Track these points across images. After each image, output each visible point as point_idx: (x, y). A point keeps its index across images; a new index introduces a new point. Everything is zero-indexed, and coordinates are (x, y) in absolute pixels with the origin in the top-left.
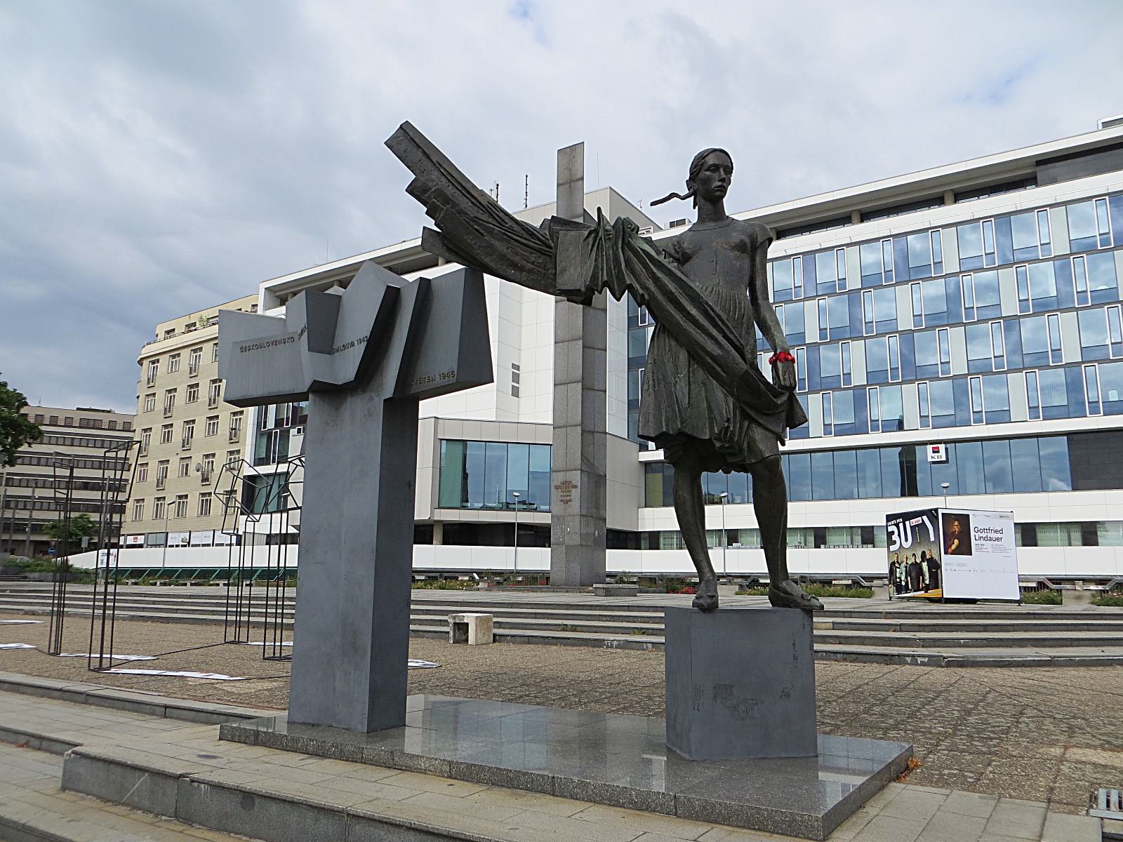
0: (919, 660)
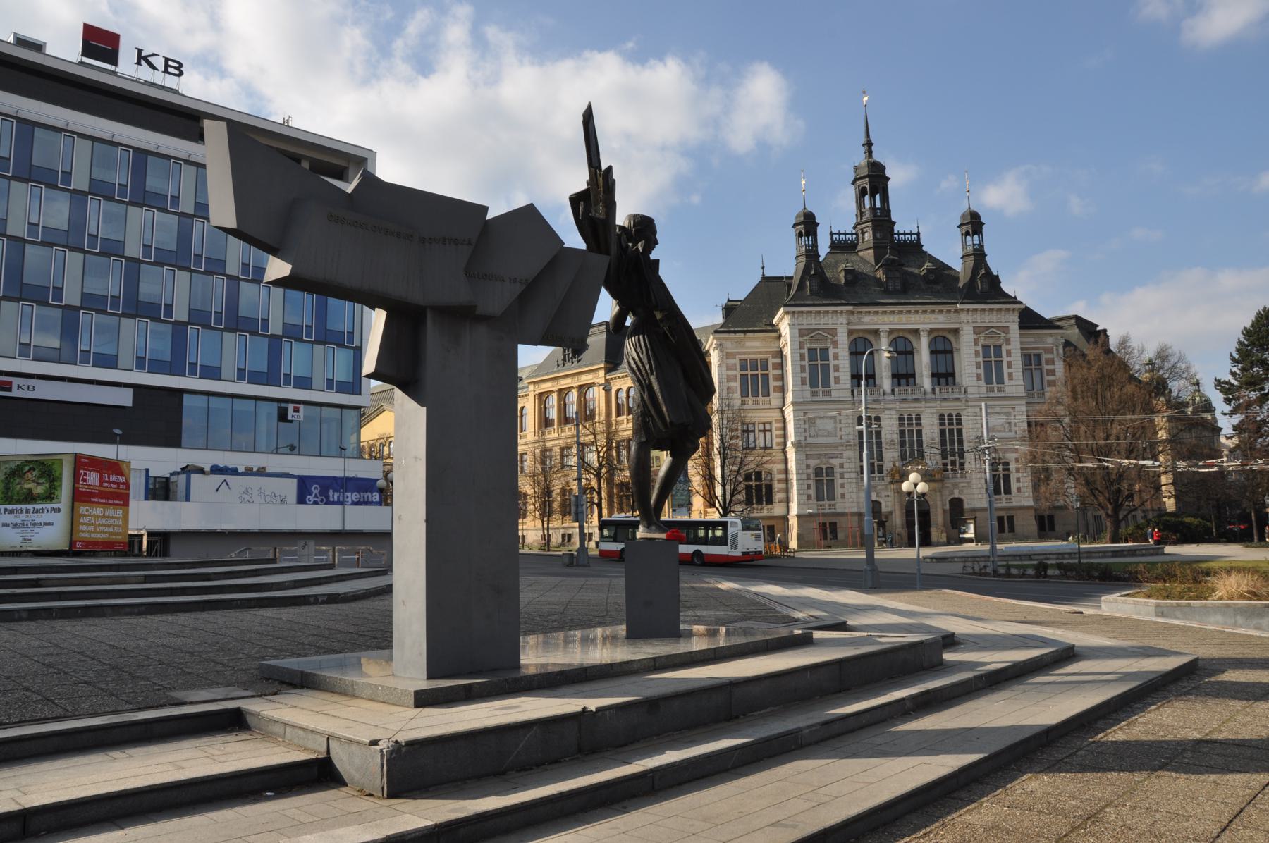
0: (320, 599)
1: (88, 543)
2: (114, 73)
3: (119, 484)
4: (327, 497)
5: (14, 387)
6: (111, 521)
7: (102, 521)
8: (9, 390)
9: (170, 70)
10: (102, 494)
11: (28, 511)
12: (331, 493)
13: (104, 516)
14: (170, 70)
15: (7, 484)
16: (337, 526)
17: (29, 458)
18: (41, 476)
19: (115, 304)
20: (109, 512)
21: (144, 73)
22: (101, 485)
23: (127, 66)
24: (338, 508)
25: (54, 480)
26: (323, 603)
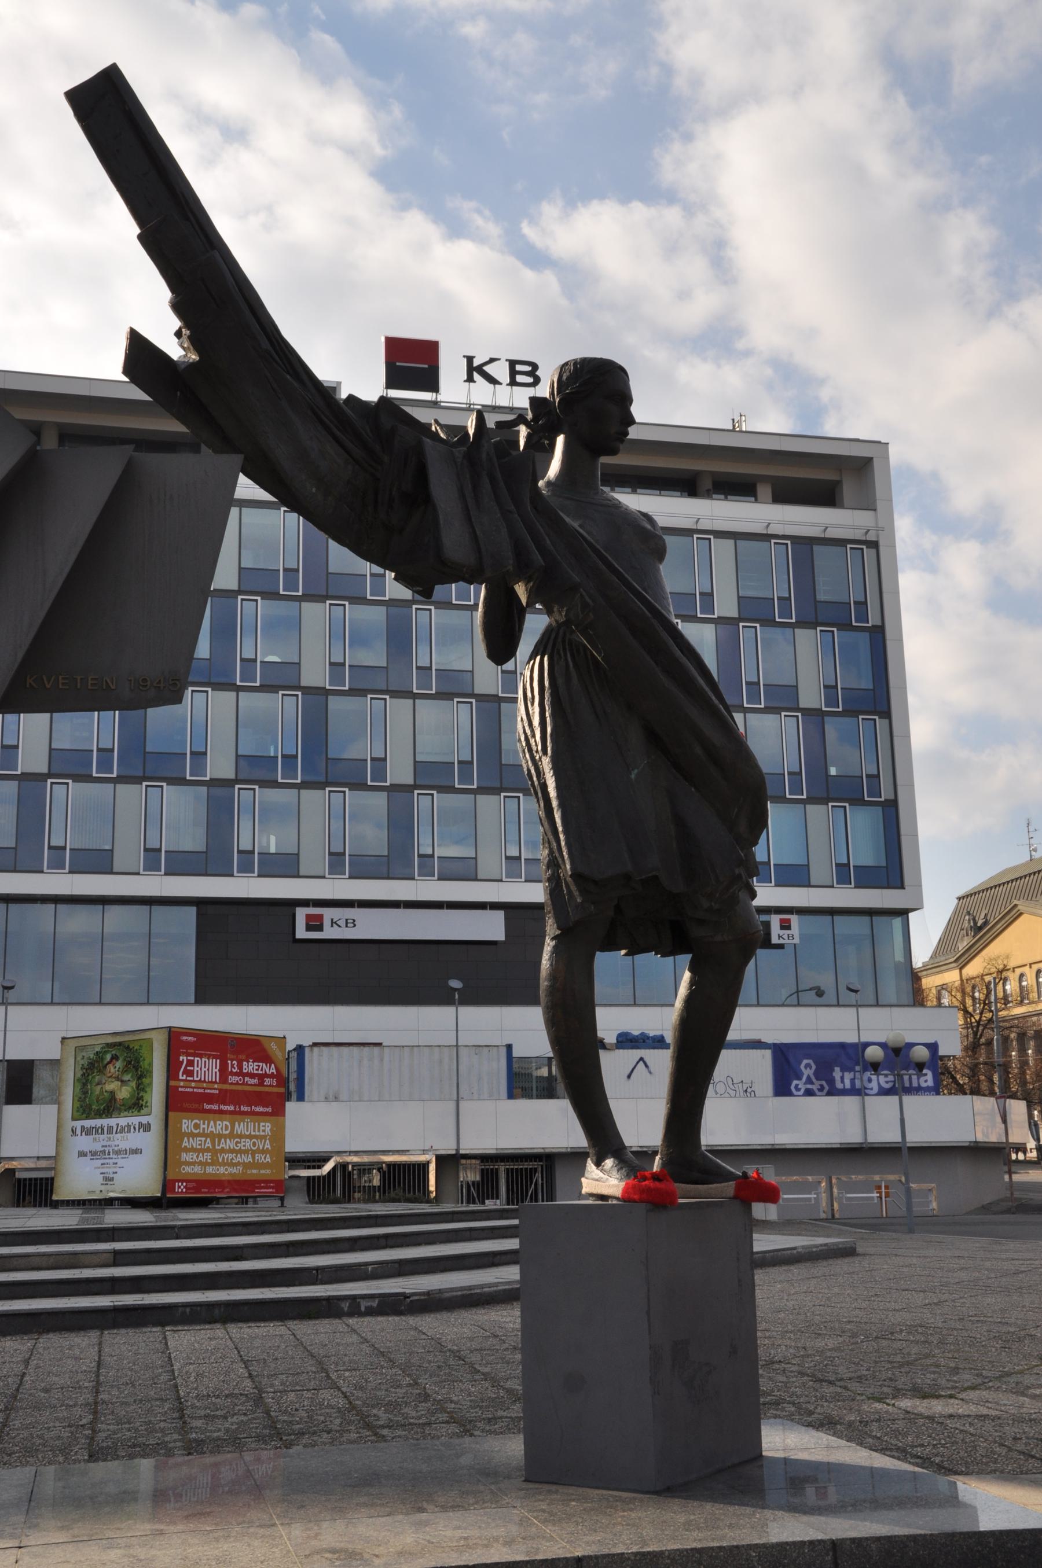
0: (364, 1305)
1: (200, 1183)
2: (435, 404)
3: (262, 1077)
4: (831, 1082)
5: (327, 923)
6: (248, 1144)
7: (230, 1144)
8: (320, 928)
9: (520, 378)
10: (223, 1097)
11: (110, 1129)
12: (837, 1073)
13: (232, 1136)
14: (520, 378)
15: (85, 1085)
16: (853, 1136)
17: (111, 1040)
18: (125, 1070)
19: (105, 764)
20: (240, 1128)
21: (482, 394)
22: (224, 1079)
23: (454, 388)
24: (851, 1102)
25: (140, 1077)
26: (370, 1312)
